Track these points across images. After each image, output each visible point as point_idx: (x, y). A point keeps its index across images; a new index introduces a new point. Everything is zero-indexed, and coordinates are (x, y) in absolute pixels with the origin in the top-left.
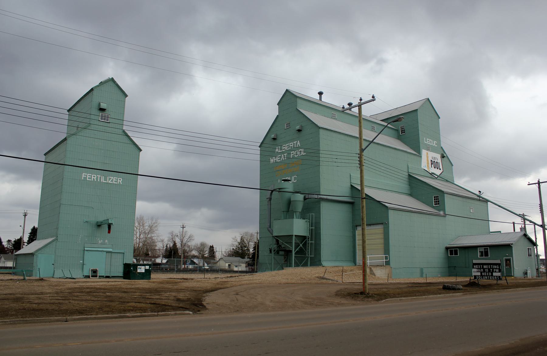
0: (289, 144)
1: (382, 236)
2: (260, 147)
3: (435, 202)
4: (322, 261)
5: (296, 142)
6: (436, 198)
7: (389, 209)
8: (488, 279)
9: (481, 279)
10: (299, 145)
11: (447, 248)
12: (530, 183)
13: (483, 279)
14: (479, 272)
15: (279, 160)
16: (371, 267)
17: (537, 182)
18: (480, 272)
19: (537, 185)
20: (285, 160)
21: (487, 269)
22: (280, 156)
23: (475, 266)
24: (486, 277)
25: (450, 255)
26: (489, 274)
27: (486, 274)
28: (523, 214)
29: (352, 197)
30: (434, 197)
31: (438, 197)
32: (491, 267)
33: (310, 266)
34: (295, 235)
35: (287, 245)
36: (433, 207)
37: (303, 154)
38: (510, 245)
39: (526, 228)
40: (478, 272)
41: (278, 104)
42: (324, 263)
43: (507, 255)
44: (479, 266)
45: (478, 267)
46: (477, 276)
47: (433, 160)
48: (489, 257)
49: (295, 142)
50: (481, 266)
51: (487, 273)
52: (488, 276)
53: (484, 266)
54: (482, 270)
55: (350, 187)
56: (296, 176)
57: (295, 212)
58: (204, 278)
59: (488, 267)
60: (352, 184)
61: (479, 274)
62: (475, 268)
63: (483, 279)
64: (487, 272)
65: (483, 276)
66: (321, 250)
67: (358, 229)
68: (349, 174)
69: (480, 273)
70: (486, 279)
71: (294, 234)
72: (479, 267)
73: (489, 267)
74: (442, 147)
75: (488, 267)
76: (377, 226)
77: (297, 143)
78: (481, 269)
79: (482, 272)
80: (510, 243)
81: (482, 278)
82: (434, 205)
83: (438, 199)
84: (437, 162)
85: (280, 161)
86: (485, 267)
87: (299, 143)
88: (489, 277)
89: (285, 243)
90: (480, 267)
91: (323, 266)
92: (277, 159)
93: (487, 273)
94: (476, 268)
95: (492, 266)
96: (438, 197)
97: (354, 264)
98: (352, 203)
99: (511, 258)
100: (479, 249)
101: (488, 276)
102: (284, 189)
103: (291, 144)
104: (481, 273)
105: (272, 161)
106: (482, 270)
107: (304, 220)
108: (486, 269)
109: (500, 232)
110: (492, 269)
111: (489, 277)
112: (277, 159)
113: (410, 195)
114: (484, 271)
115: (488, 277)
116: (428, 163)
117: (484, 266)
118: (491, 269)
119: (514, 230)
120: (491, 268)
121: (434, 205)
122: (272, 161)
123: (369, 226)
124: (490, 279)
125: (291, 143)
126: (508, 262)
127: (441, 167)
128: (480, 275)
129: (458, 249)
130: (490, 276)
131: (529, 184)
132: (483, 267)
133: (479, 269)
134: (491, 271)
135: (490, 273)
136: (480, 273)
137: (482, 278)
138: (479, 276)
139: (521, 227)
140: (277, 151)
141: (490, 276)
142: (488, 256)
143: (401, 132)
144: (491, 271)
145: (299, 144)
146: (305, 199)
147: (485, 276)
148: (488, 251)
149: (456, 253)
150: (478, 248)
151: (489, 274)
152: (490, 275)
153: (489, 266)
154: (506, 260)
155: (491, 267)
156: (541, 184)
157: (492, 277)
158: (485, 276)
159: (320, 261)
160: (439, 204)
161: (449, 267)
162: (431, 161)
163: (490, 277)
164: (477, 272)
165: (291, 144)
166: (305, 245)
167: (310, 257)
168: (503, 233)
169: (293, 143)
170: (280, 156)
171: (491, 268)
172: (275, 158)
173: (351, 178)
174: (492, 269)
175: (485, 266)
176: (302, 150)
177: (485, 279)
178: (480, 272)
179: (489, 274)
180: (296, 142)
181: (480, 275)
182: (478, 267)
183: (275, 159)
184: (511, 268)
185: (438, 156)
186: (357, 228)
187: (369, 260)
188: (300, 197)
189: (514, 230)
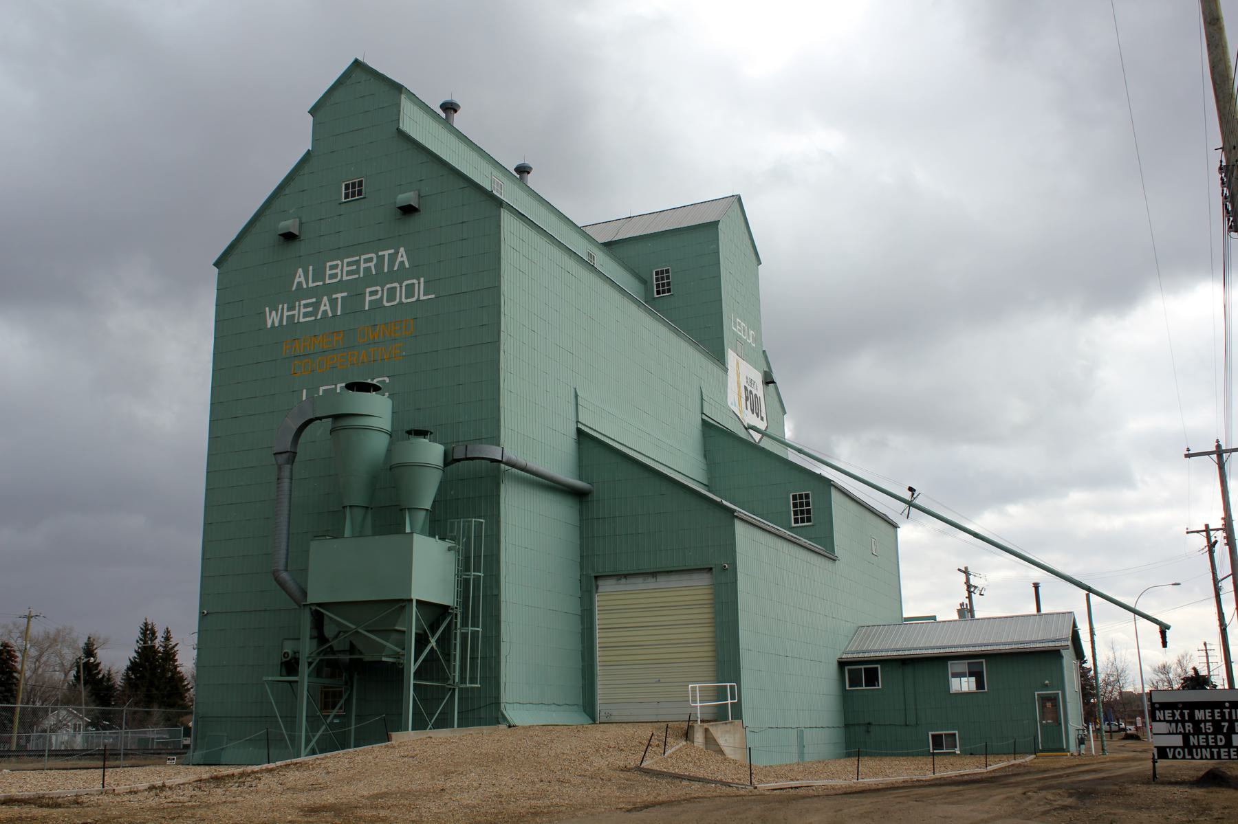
0: (357, 258)
1: (705, 614)
2: (217, 264)
3: (796, 513)
4: (502, 706)
5: (392, 251)
6: (802, 502)
7: (736, 517)
8: (1212, 758)
9: (1184, 758)
10: (402, 262)
11: (842, 664)
12: (1190, 452)
13: (1193, 758)
14: (1177, 734)
15: (306, 315)
16: (706, 725)
17: (1214, 449)
18: (1180, 733)
19: (1214, 457)
20: (335, 316)
21: (1209, 721)
22: (314, 300)
23: (1159, 715)
24: (1206, 753)
25: (850, 686)
26: (1215, 739)
27: (1207, 739)
28: (966, 568)
29: (581, 473)
30: (794, 497)
31: (807, 496)
32: (1223, 714)
33: (458, 726)
34: (418, 601)
35: (378, 639)
36: (791, 529)
37: (422, 298)
38: (1059, 650)
39: (975, 609)
40: (1173, 734)
41: (313, 111)
42: (513, 713)
43: (1047, 682)
44: (1177, 713)
45: (1174, 715)
46: (1170, 748)
47: (749, 388)
48: (986, 690)
49: (386, 253)
50: (1186, 712)
51: (1210, 737)
52: (1211, 747)
53: (1197, 712)
54: (1187, 729)
55: (573, 433)
56: (387, 380)
57: (408, 509)
58: (103, 792)
59: (1213, 715)
60: (580, 426)
61: (1178, 741)
62: (1160, 721)
63: (1230, 758)
64: (1207, 734)
65: (1194, 746)
66: (499, 663)
67: (600, 589)
68: (573, 391)
69: (1181, 736)
70: (1206, 759)
71: (416, 595)
72: (1178, 717)
73: (1216, 715)
74: (764, 351)
75: (1213, 715)
76: (674, 578)
77: (393, 258)
78: (1183, 722)
79: (1190, 733)
80: (1057, 644)
81: (1190, 753)
82: (793, 525)
83: (808, 504)
84: (756, 395)
85: (313, 318)
86: (1199, 715)
87: (402, 257)
88: (1215, 750)
89: (368, 631)
90: (1182, 715)
91: (510, 727)
92: (296, 312)
93: (1210, 737)
94: (1165, 721)
95: (1226, 711)
96: (807, 496)
97: (591, 722)
98: (578, 495)
99: (1060, 692)
100: (951, 664)
101: (1211, 747)
102: (357, 418)
103: (368, 262)
104: (1186, 737)
105: (272, 319)
106: (1189, 727)
107: (448, 544)
108: (1205, 721)
109: (934, 618)
110: (1226, 724)
111: (1215, 750)
112: (301, 313)
113: (706, 488)
114: (1198, 731)
115: (1212, 753)
116: (740, 396)
117: (1197, 711)
118: (1226, 721)
119: (1039, 609)
120: (1224, 720)
121: (793, 525)
122: (272, 319)
123: (651, 580)
124: (1219, 757)
125: (363, 257)
126: (1049, 705)
127: (764, 415)
128: (1181, 744)
129: (879, 666)
130: (1220, 747)
131: (1187, 453)
132: (1192, 715)
133: (1177, 722)
134: (1225, 731)
135: (1219, 737)
136: (1181, 736)
137: (1190, 753)
138: (1175, 748)
139: (960, 608)
140: (300, 284)
141: (1220, 747)
142: (984, 689)
143: (655, 290)
144: (1225, 731)
145: (405, 259)
146: (449, 460)
147: (1201, 747)
148: (983, 672)
149: (871, 678)
150: (949, 663)
151: (1216, 742)
152: (1219, 744)
153: (1216, 711)
154: (1044, 699)
155: (1223, 714)
156: (1225, 455)
157: (1229, 752)
158: (1201, 747)
159: (496, 703)
160: (809, 520)
161: (847, 726)
162: (746, 388)
163: (1222, 750)
164: (1169, 734)
165: (370, 260)
166: (445, 641)
167: (461, 690)
168: (940, 622)
169: (378, 257)
170: (314, 300)
171: (1224, 720)
172: (291, 308)
173: (577, 404)
174: (1226, 724)
175: (1202, 711)
176: (420, 285)
177: (1201, 758)
178: (1180, 733)
179: (1215, 739)
180: (392, 251)
181: (1181, 744)
182: (1174, 715)
183: (286, 314)
184: (1060, 724)
185: (758, 378)
186: (597, 587)
187: (697, 706)
188: (432, 452)
189: (1039, 609)
